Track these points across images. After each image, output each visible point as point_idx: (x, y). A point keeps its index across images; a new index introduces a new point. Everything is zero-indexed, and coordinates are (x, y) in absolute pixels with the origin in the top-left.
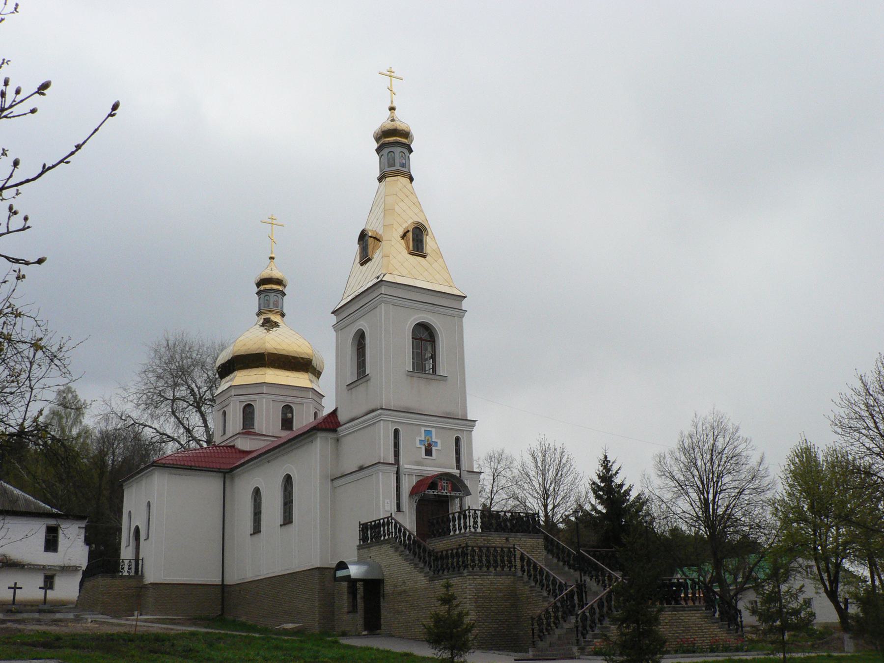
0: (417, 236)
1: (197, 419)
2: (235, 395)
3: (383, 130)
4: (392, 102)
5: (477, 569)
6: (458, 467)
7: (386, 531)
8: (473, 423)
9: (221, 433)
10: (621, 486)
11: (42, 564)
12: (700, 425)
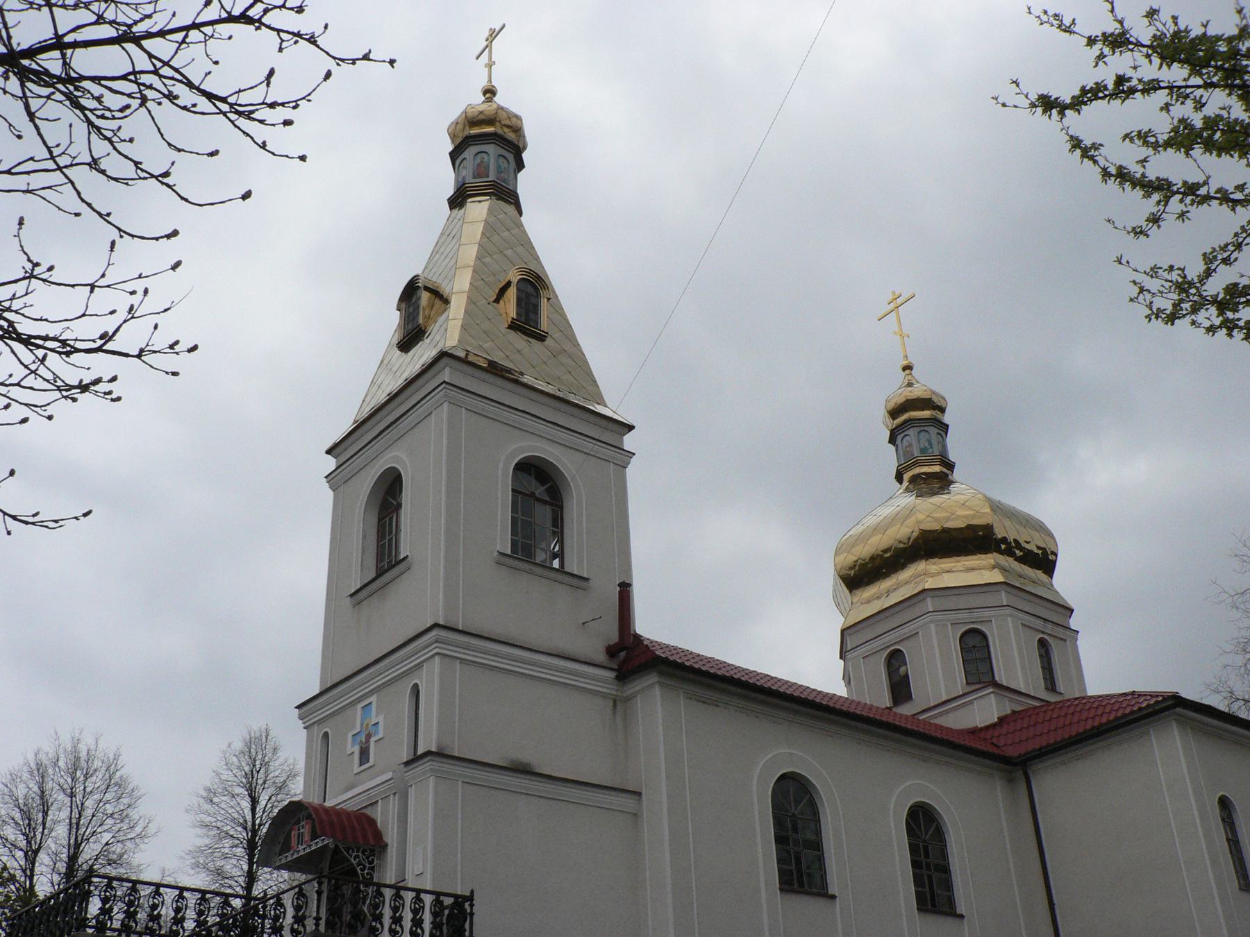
4: (490, 81)
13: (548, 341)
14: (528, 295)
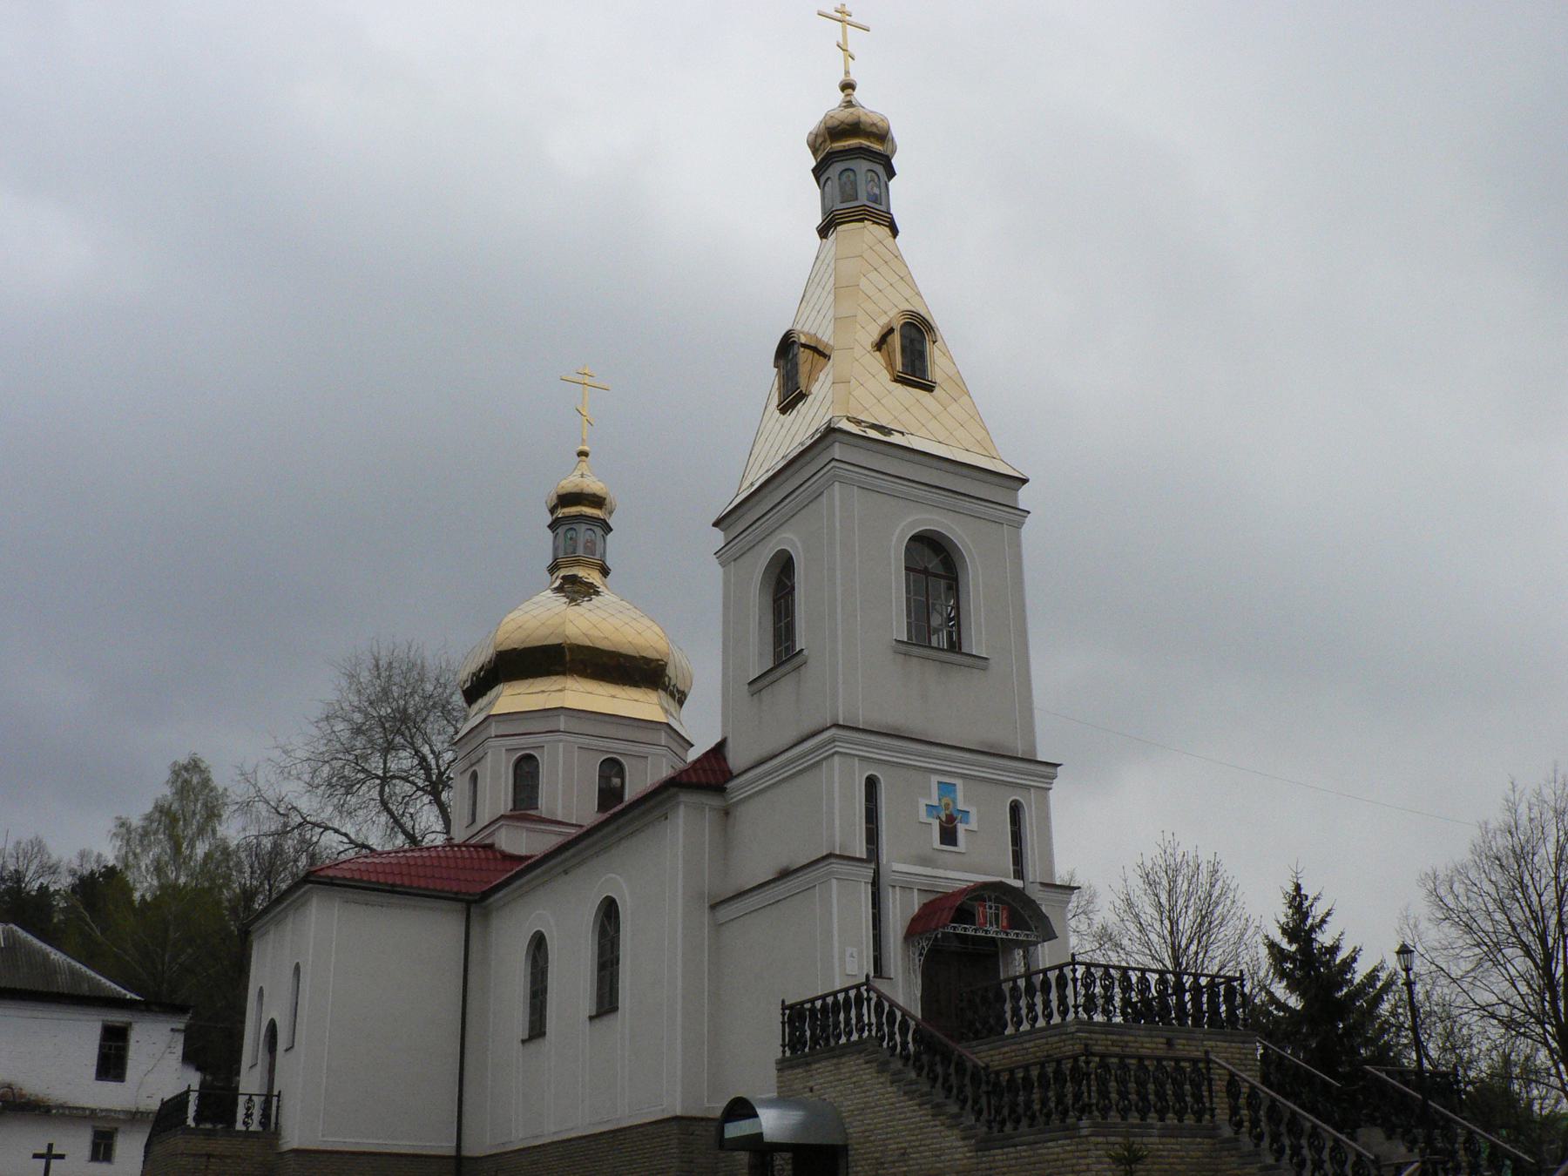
0: (912, 341)
1: (432, 819)
2: (496, 736)
4: (847, 73)
5: (1114, 1117)
6: (1019, 874)
7: (854, 1021)
8: (1050, 770)
9: (466, 821)
10: (1334, 949)
11: (89, 1105)
12: (1523, 808)
13: (937, 391)
14: (912, 341)
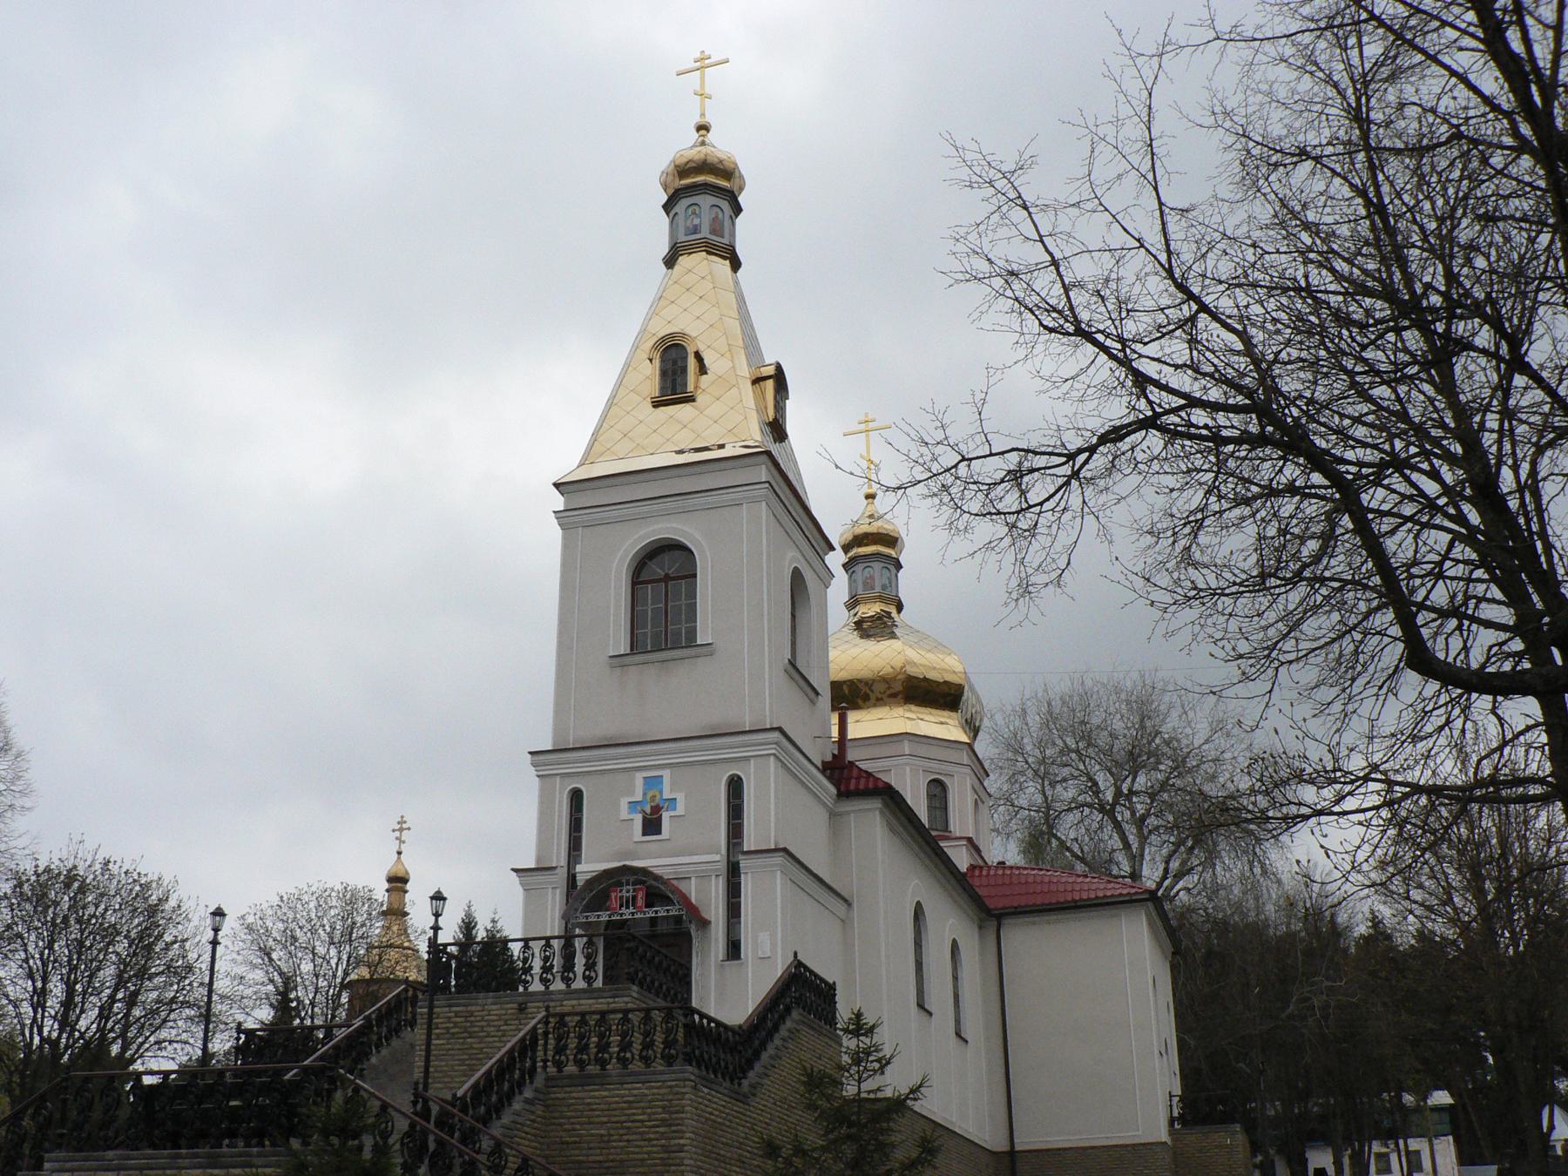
3: (677, 163)
4: (703, 115)
